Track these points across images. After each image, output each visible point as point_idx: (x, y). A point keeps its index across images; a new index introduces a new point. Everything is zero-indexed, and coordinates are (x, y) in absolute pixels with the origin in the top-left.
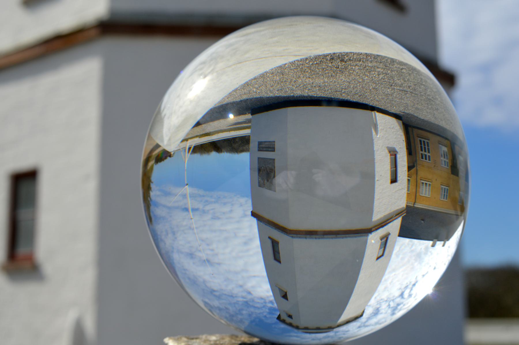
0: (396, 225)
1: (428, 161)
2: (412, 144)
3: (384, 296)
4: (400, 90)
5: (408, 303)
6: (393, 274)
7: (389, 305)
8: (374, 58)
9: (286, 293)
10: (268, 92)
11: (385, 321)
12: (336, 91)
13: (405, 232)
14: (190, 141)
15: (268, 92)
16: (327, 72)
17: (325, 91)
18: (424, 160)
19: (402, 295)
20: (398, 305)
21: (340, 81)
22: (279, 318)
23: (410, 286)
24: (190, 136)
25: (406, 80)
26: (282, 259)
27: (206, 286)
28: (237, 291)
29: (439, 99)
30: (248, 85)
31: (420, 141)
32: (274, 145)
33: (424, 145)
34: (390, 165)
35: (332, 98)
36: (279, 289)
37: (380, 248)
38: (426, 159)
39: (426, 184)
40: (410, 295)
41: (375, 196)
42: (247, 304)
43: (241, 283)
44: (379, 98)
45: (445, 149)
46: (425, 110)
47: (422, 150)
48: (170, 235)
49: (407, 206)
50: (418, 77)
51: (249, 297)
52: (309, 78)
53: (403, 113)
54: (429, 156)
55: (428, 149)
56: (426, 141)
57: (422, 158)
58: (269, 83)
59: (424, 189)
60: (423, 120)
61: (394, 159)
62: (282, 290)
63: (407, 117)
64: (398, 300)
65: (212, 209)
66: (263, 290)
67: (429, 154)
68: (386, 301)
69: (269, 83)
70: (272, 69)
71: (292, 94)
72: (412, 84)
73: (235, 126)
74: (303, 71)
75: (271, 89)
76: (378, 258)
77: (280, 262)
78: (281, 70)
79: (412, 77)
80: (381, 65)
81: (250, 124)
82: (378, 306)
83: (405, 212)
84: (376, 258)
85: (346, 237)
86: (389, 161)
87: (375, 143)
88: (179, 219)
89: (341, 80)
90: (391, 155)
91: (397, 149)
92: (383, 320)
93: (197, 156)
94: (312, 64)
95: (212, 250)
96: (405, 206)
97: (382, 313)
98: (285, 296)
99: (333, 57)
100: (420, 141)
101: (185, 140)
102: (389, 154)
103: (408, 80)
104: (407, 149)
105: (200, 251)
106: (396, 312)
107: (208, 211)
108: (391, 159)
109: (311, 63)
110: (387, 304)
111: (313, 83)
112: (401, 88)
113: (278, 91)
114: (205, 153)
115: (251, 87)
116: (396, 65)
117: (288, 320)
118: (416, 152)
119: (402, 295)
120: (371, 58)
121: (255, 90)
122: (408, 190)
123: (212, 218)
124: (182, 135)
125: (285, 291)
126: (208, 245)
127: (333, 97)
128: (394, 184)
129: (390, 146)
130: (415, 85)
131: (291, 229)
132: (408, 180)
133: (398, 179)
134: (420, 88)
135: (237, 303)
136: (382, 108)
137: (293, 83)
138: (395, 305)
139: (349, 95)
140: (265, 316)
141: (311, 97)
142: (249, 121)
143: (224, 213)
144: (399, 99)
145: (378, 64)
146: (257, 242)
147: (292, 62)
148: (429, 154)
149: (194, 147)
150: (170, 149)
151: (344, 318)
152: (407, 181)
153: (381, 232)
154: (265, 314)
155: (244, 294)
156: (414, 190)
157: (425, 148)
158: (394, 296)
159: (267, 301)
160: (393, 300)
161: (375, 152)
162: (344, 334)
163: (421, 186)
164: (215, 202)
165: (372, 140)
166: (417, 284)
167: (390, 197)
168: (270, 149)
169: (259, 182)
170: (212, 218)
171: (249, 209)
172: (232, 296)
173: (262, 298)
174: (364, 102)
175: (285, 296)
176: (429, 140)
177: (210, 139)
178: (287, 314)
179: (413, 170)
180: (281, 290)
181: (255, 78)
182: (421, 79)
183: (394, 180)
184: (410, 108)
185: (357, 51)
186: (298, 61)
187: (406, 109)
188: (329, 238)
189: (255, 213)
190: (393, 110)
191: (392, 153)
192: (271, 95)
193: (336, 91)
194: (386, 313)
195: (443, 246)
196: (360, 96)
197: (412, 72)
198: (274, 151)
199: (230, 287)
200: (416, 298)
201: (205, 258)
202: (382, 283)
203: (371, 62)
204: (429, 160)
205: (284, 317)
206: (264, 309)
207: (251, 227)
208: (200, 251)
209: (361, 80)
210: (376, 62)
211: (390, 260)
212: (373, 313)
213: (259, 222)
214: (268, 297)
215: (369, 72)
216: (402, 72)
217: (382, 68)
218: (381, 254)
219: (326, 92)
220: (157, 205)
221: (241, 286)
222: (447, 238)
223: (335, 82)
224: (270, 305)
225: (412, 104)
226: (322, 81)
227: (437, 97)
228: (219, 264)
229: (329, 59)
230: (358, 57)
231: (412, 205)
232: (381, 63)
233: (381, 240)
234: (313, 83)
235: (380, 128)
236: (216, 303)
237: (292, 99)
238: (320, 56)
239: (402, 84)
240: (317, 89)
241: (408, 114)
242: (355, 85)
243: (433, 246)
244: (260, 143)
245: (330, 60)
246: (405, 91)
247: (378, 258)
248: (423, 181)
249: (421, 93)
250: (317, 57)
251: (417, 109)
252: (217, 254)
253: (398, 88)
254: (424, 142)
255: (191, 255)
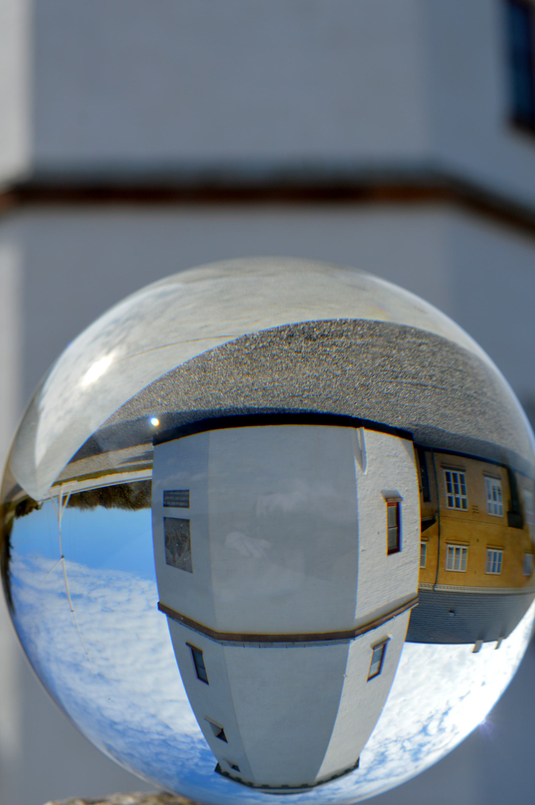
0: (403, 619)
1: (461, 509)
2: (431, 482)
3: (391, 733)
4: (413, 385)
5: (441, 742)
6: (402, 699)
7: (403, 748)
8: (369, 329)
9: (222, 730)
10: (181, 403)
11: (406, 771)
12: (294, 396)
13: (419, 633)
14: (65, 485)
15: (181, 403)
16: (279, 360)
17: (273, 397)
18: (454, 508)
19: (424, 730)
20: (421, 745)
21: (301, 376)
22: (218, 769)
23: (439, 716)
24: (64, 478)
25: (427, 363)
26: (209, 679)
27: (102, 715)
28: (148, 723)
29: (489, 394)
30: (150, 392)
31: (448, 474)
32: (188, 496)
33: (455, 480)
34: (386, 523)
35: (284, 410)
36: (211, 723)
37: (373, 662)
38: (458, 506)
39: (457, 549)
40: (441, 730)
41: (360, 578)
42: (165, 743)
43: (152, 711)
44: (371, 403)
45: (497, 483)
46: (460, 416)
47: (449, 491)
48: (43, 634)
49: (420, 590)
50: (451, 357)
51: (168, 733)
52: (248, 374)
53: (417, 425)
54: (464, 501)
55: (463, 488)
56: (459, 473)
57: (451, 504)
58: (182, 386)
59: (454, 559)
60: (455, 435)
61: (394, 512)
62: (218, 727)
63: (423, 433)
64: (420, 739)
65: (102, 597)
66: (185, 723)
67: (464, 497)
68: (396, 741)
69: (182, 386)
70: (188, 362)
71: (218, 407)
72: (437, 372)
73: (129, 464)
74: (238, 363)
75: (185, 398)
76: (370, 679)
77: (206, 682)
78: (202, 365)
79: (439, 357)
80: (381, 341)
81: (151, 461)
82: (382, 750)
83: (417, 600)
84: (367, 678)
85: (305, 646)
86: (385, 515)
87: (359, 486)
88: (56, 611)
89: (304, 374)
90: (389, 505)
91: (401, 494)
92: (400, 770)
93: (75, 511)
94: (255, 349)
95: (107, 659)
96: (416, 591)
97: (392, 760)
98: (221, 735)
99: (290, 333)
100: (448, 474)
101: (58, 483)
102: (386, 504)
103: (430, 364)
104: (420, 491)
105: (88, 660)
106: (421, 755)
107: (96, 599)
108: (389, 512)
109: (253, 347)
110: (399, 745)
111: (253, 384)
112: (415, 381)
113: (195, 401)
114: (86, 507)
115: (154, 396)
116: (409, 338)
117: (233, 773)
118: (438, 495)
119: (424, 730)
120: (362, 329)
121: (159, 400)
122: (422, 563)
123: (102, 610)
124: (53, 475)
125: (221, 727)
126: (100, 651)
127: (286, 407)
128: (395, 555)
129: (387, 488)
130: (443, 372)
131: (220, 632)
132: (423, 546)
133: (403, 545)
134: (452, 377)
135: (150, 743)
136: (377, 420)
137: (220, 386)
138: (416, 747)
139: (315, 402)
140: (196, 765)
141: (248, 409)
142: (148, 456)
143: (119, 603)
144: (410, 401)
145: (375, 338)
146: (170, 650)
147: (222, 347)
148: (464, 497)
149: (72, 496)
150: (37, 495)
151: (324, 771)
152: (419, 547)
153: (374, 636)
154: (196, 760)
155: (160, 728)
156: (434, 563)
157: (456, 487)
158: (409, 734)
159: (196, 740)
160: (409, 740)
161: (359, 502)
162: (334, 794)
163: (448, 554)
164: (105, 586)
165: (354, 481)
166: (450, 713)
167: (387, 578)
168: (181, 504)
169: (167, 558)
170: (102, 610)
171: (156, 600)
172: (142, 732)
173: (186, 736)
174: (342, 413)
175: (221, 735)
176: (464, 471)
177: (94, 484)
178: (229, 763)
179: (432, 528)
180: (214, 726)
181: (161, 379)
182: (457, 360)
183: (394, 548)
184: (429, 416)
185: (338, 318)
186: (231, 343)
187: (423, 418)
188: (282, 647)
189: (163, 606)
190: (396, 423)
191: (391, 501)
192: (185, 409)
193: (294, 396)
194: (401, 759)
195: (497, 648)
196: (335, 402)
197: (440, 349)
198: (187, 506)
199: (137, 718)
200: (456, 731)
201: (96, 671)
202: (383, 714)
203: (362, 336)
204: (464, 507)
205: (226, 768)
206: (192, 752)
207: (159, 626)
208: (88, 660)
209: (339, 372)
210: (371, 335)
211: (392, 680)
212: (375, 760)
213: (171, 620)
214: (196, 734)
215: (356, 356)
216: (418, 351)
217: (382, 346)
218: (375, 671)
219: (275, 399)
220: (20, 585)
221: (154, 716)
222: (501, 633)
223: (292, 379)
224: (200, 746)
225: (434, 408)
226: (269, 379)
227: (485, 390)
228: (118, 681)
229: (285, 336)
230: (339, 328)
231: (431, 589)
232: (380, 336)
233: (374, 648)
234: (253, 384)
235: (369, 457)
236: (120, 744)
237: (217, 415)
238: (270, 332)
239: (417, 373)
240: (260, 393)
241: (426, 427)
242: (328, 382)
243: (476, 651)
244: (167, 493)
245: (287, 338)
246: (421, 385)
247: (370, 679)
248: (451, 546)
249: (453, 386)
250: (265, 334)
251: (443, 416)
252: (113, 666)
253: (410, 380)
254: (455, 475)
255: (76, 667)
